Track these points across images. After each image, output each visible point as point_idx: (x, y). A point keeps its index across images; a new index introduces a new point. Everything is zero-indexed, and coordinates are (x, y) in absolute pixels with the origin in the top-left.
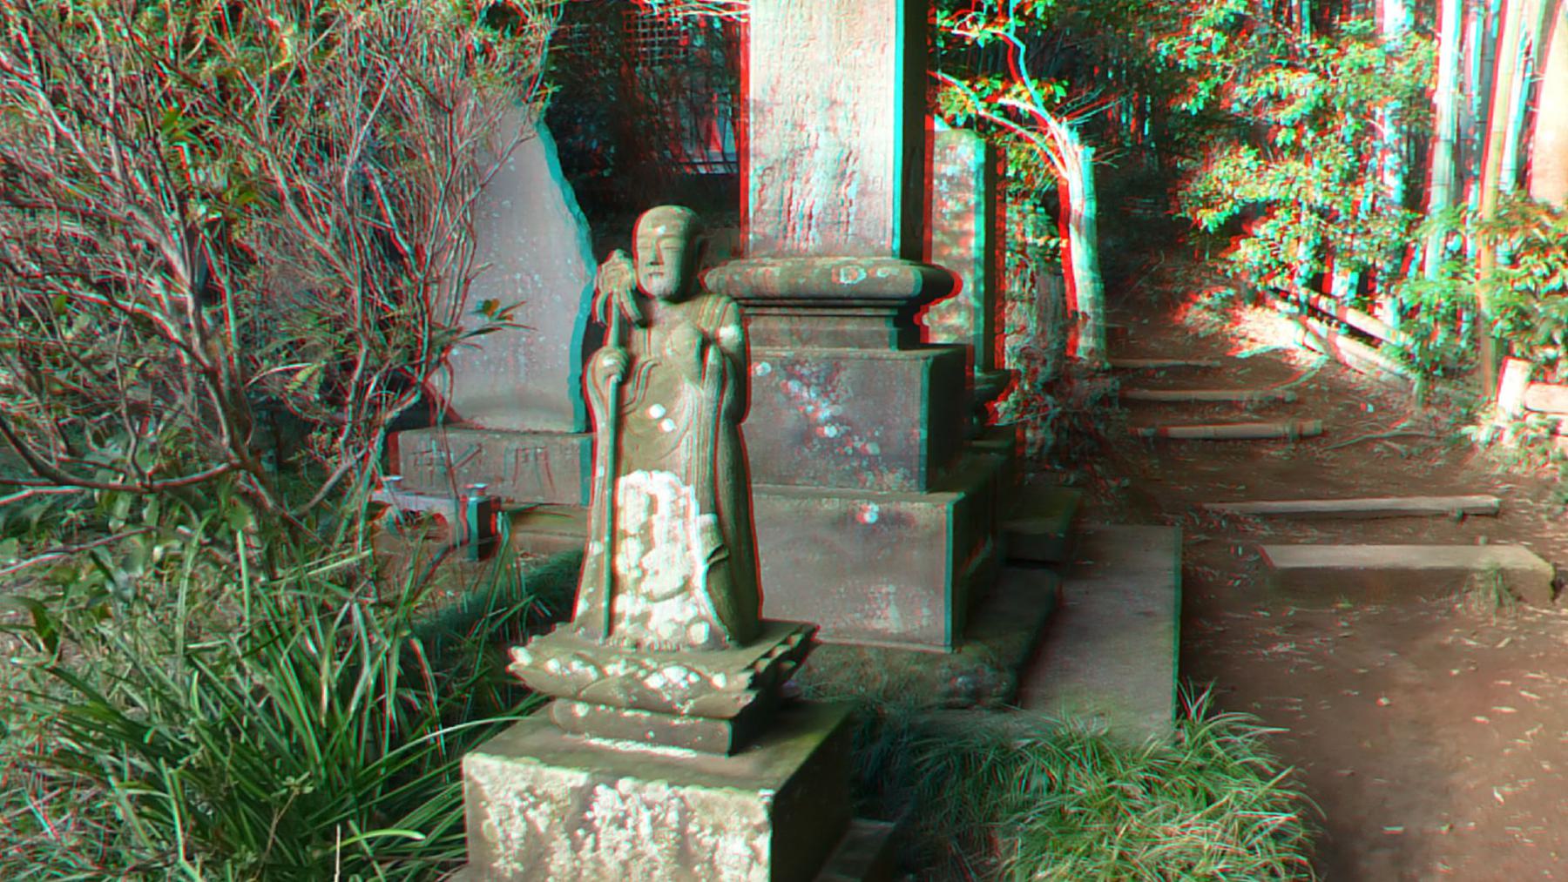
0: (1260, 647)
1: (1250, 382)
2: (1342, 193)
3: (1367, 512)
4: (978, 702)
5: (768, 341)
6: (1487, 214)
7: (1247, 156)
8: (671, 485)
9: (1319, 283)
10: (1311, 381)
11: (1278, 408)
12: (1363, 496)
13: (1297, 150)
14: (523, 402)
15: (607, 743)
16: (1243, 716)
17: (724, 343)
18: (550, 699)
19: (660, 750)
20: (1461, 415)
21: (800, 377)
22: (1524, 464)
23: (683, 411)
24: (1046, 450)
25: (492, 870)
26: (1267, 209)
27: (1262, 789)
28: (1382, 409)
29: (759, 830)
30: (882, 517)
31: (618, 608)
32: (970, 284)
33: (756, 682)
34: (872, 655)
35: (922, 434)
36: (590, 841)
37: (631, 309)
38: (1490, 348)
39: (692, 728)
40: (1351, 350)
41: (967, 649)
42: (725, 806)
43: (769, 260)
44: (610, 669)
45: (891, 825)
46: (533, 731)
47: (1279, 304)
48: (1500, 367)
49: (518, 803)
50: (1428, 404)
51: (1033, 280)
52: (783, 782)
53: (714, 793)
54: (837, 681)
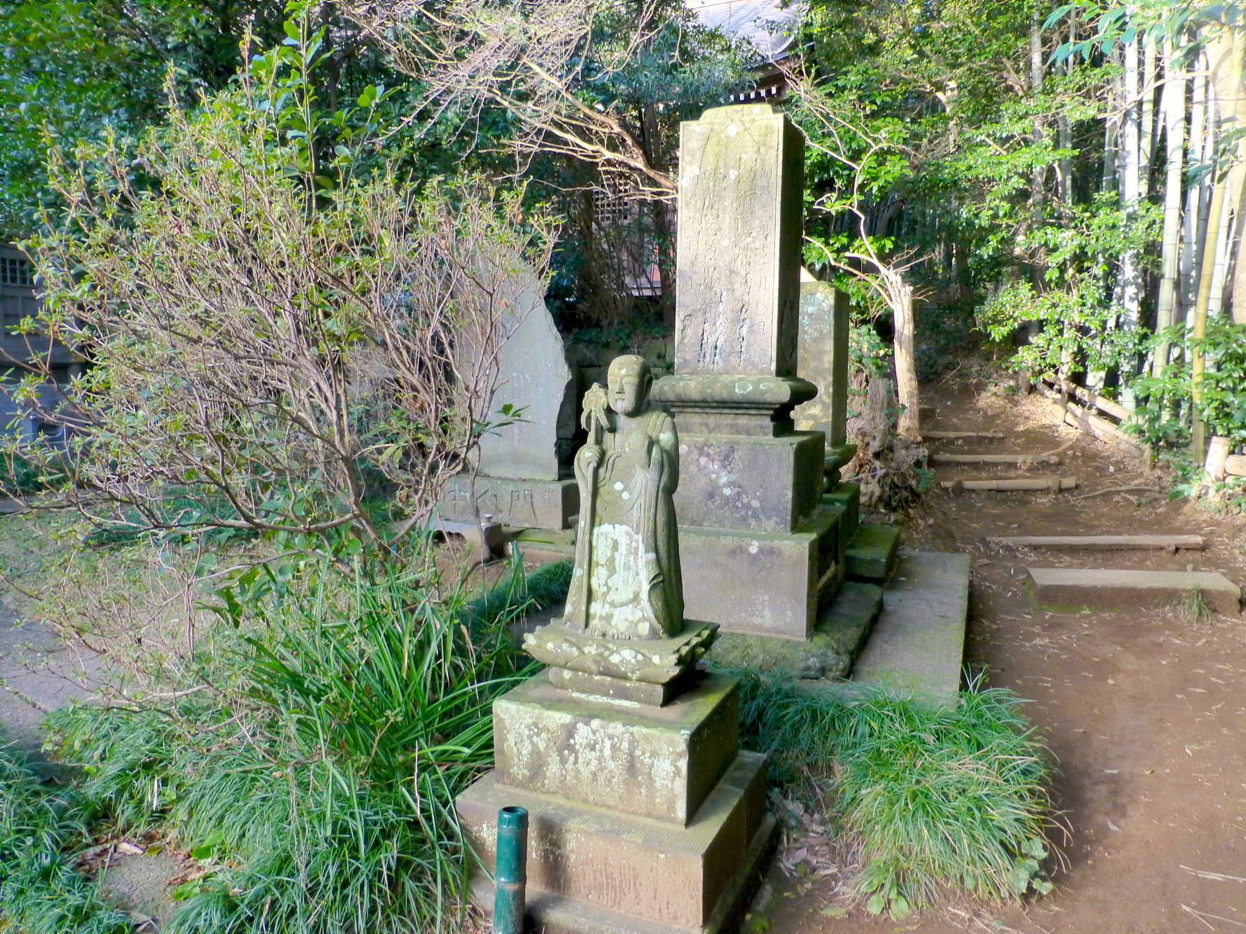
0: (1024, 640)
1: (1025, 449)
2: (1093, 314)
3: (1105, 545)
4: (823, 675)
5: (687, 430)
6: (1199, 334)
7: (1024, 288)
8: (627, 533)
9: (1079, 378)
10: (1071, 448)
11: (1043, 468)
12: (1103, 533)
13: (1061, 283)
14: (516, 459)
15: (583, 696)
16: (1007, 690)
17: (662, 444)
18: (544, 666)
19: (617, 702)
20: (1176, 477)
21: (708, 455)
22: (1223, 513)
23: (634, 487)
24: (874, 499)
25: (509, 774)
26: (1041, 325)
27: (1016, 740)
28: (1120, 470)
29: (680, 755)
30: (761, 550)
31: (592, 611)
32: (824, 388)
33: (680, 661)
34: (752, 641)
35: (790, 494)
36: (572, 758)
37: (604, 422)
38: (1199, 430)
39: (638, 689)
40: (1100, 427)
41: (816, 639)
42: (659, 739)
43: (688, 377)
44: (586, 650)
45: (765, 756)
46: (536, 687)
47: (1048, 392)
48: (1207, 441)
49: (527, 732)
50: (1154, 467)
51: (867, 381)
52: (695, 727)
53: (652, 731)
54: (731, 657)
